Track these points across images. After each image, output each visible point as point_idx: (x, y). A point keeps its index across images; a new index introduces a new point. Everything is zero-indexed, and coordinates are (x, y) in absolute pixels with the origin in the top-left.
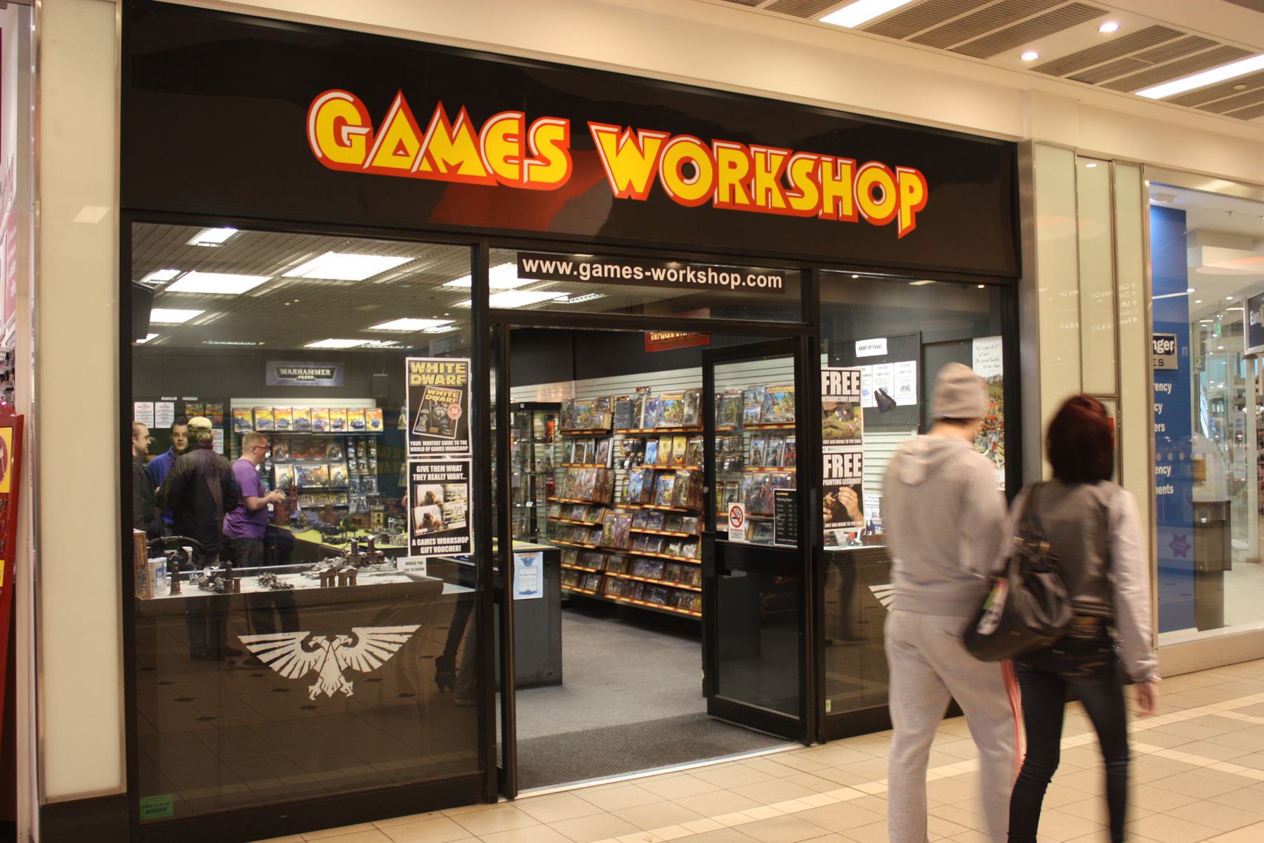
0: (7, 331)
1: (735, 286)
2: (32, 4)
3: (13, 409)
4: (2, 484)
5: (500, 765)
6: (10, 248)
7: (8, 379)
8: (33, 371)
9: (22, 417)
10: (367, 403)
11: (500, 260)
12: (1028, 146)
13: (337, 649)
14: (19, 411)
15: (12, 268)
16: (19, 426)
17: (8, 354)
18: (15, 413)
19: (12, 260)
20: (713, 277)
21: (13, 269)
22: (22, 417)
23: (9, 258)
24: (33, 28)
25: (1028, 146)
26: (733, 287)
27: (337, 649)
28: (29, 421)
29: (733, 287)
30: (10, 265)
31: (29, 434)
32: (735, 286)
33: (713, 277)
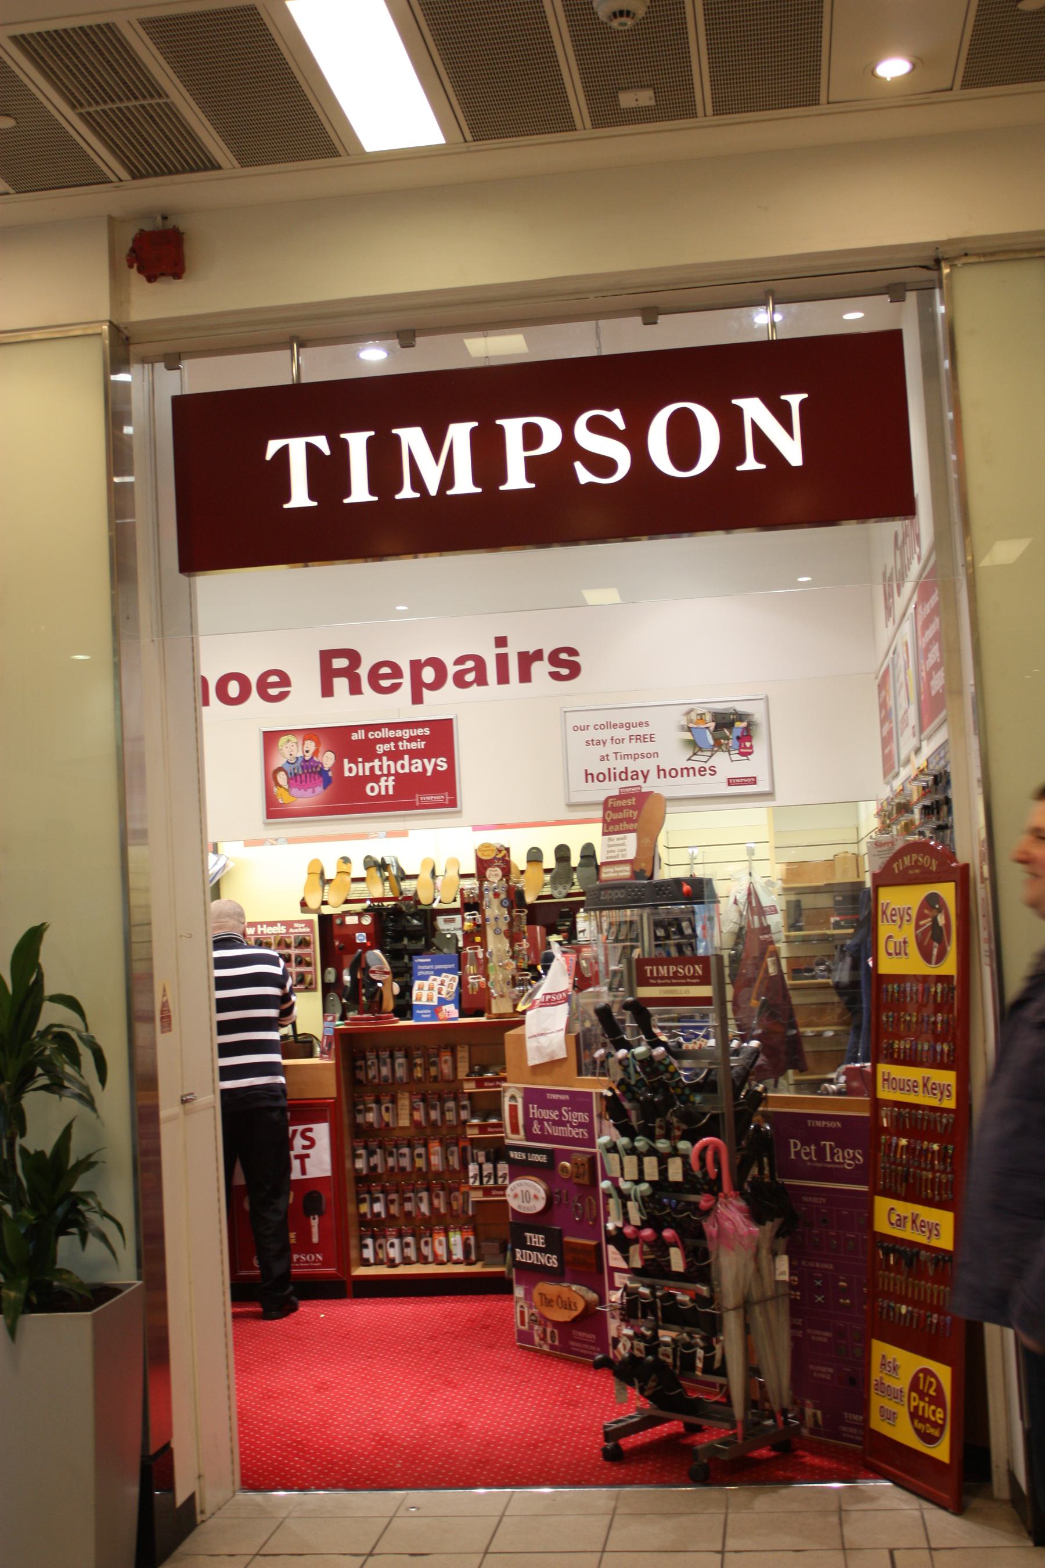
0: (924, 743)
1: (403, 759)
2: (937, 285)
3: (952, 856)
4: (1037, 947)
5: (5, 1156)
6: (926, 625)
7: (938, 813)
8: (980, 790)
9: (966, 867)
10: (882, 1225)
11: (259, 1089)
12: (710, 881)
13: (362, 1555)
14: (962, 857)
15: (930, 655)
16: (963, 877)
17: (936, 777)
18: (956, 861)
19: (930, 643)
20: (389, 766)
21: (934, 655)
22: (966, 867)
23: (923, 642)
24: (941, 309)
25: (710, 881)
26: (406, 757)
27: (362, 1555)
28: (980, 870)
29: (406, 757)
30: (927, 650)
31: (981, 892)
32: (403, 759)
33: (389, 766)
